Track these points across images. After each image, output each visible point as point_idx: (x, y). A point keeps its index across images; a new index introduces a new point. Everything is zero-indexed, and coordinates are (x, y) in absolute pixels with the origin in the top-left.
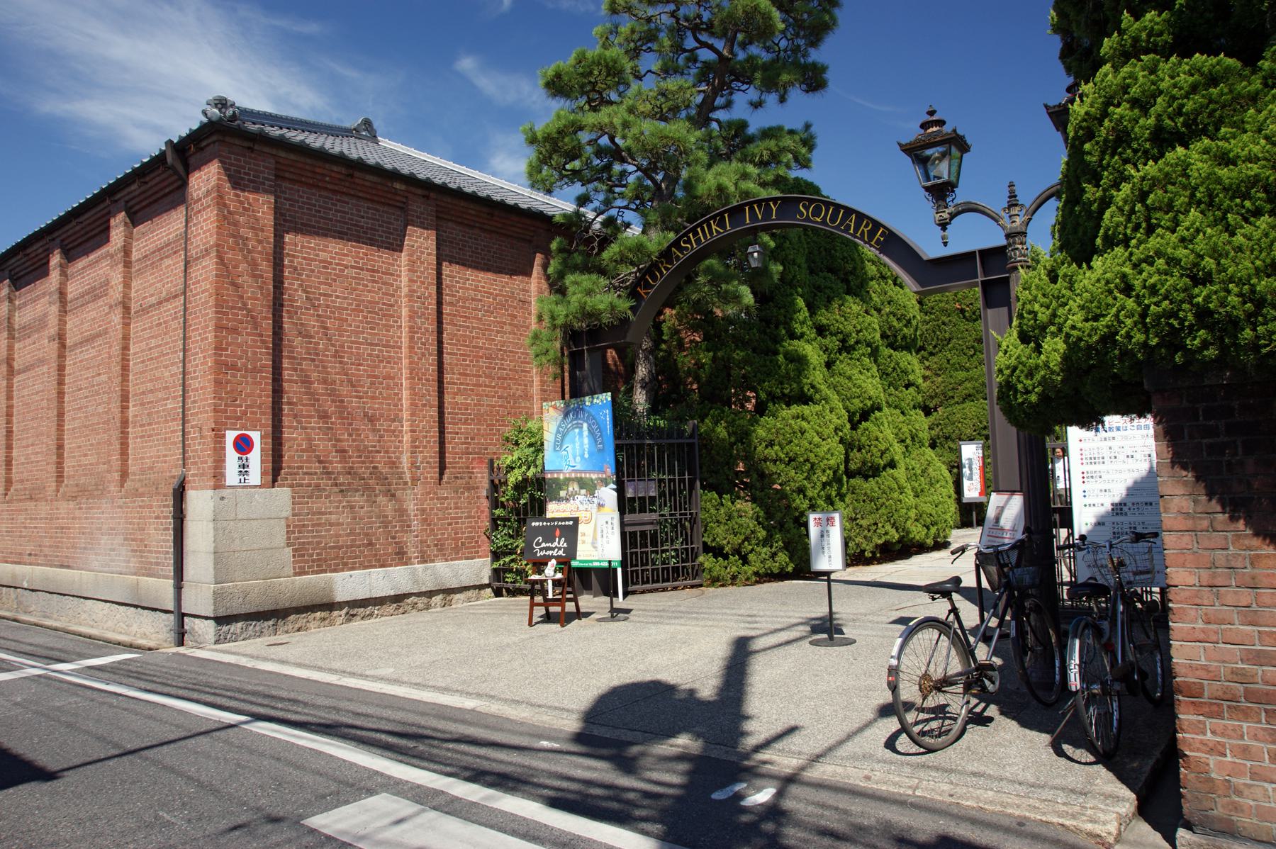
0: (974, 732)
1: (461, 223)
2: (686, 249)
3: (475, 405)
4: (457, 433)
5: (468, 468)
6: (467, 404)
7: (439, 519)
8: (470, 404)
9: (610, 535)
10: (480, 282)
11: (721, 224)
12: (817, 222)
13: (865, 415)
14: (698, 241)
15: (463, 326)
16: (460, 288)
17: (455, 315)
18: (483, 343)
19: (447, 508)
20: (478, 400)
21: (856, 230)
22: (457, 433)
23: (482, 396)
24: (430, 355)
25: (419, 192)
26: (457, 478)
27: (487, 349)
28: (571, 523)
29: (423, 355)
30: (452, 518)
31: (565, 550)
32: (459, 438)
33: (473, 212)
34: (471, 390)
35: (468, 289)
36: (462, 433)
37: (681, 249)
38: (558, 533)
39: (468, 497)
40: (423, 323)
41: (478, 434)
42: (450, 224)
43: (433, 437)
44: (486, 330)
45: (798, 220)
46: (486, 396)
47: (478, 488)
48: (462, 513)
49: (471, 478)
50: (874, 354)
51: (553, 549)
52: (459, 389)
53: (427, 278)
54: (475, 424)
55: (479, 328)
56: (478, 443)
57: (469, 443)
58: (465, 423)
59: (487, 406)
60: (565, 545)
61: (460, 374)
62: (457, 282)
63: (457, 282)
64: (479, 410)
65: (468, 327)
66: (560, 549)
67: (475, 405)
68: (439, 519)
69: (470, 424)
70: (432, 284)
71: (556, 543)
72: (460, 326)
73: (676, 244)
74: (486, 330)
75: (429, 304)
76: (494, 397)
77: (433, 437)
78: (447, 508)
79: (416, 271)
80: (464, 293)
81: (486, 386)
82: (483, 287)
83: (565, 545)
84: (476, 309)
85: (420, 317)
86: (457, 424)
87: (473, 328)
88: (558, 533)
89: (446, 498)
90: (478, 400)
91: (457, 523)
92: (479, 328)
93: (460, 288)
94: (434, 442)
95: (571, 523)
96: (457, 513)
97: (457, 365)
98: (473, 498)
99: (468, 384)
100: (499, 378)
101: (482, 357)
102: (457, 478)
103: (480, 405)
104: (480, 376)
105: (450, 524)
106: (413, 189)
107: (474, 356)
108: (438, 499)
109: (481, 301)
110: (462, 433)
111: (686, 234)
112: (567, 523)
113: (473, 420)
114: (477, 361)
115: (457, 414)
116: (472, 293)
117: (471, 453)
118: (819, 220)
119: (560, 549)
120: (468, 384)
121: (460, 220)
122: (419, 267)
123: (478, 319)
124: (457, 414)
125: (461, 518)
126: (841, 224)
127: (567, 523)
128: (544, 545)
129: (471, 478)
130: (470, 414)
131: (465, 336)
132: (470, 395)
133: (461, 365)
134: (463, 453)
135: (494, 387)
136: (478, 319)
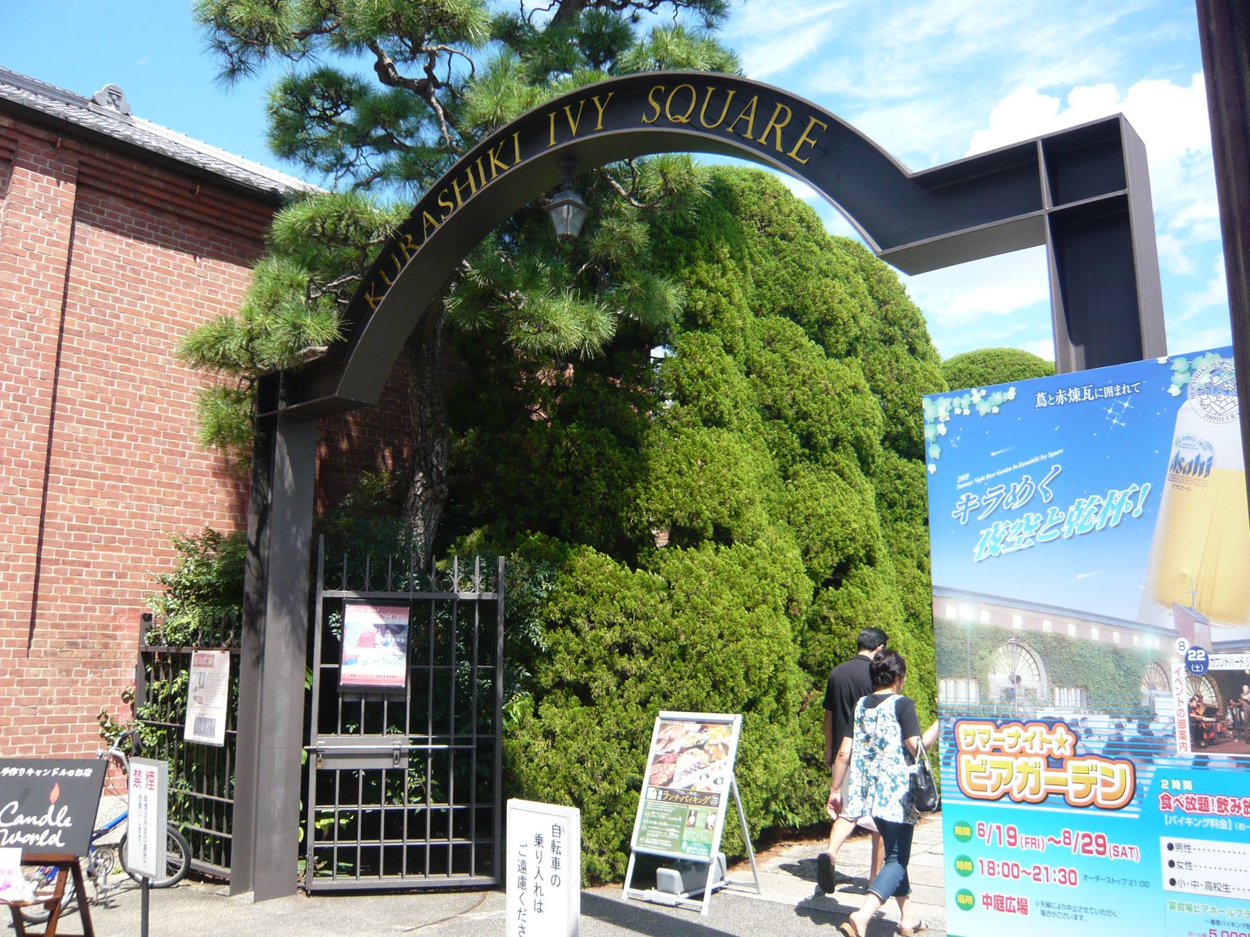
0: (1072, 920)
1: (136, 202)
2: (446, 210)
3: (133, 516)
4: (88, 565)
5: (105, 627)
6: (114, 513)
7: (20, 721)
8: (122, 514)
9: (546, 885)
10: (167, 304)
11: (506, 157)
12: (680, 125)
13: (841, 573)
14: (466, 193)
15: (122, 377)
16: (123, 311)
17: (105, 356)
18: (161, 409)
19: (41, 702)
20: (139, 508)
21: (758, 132)
22: (88, 565)
23: (149, 500)
24: (32, 419)
25: (43, 134)
26: (75, 645)
27: (168, 419)
28: (88, 772)
29: (18, 418)
30: (51, 720)
31: (66, 835)
32: (89, 574)
33: (161, 185)
34: (126, 489)
35: (139, 314)
36: (97, 565)
37: (437, 212)
38: (55, 794)
39: (93, 682)
40: (22, 362)
41: (135, 568)
42: (112, 201)
43: (23, 568)
44: (171, 387)
45: (645, 124)
46: (160, 501)
47: (116, 665)
48: (76, 710)
49: (106, 646)
50: (865, 462)
51: (38, 830)
52: (99, 486)
53: (44, 284)
54: (129, 550)
55: (158, 384)
56: (135, 585)
57: (114, 584)
58: (105, 548)
59: (160, 518)
60: (67, 823)
61: (105, 459)
62: (116, 300)
63: (116, 300)
64: (142, 525)
65: (132, 379)
66: (54, 830)
67: (133, 516)
68: (20, 721)
69: (119, 549)
70: (53, 296)
71: (48, 818)
72: (114, 376)
73: (428, 204)
74: (171, 387)
75: (45, 330)
76: (177, 503)
77: (23, 568)
78: (41, 702)
79: (21, 271)
80: (131, 320)
81: (160, 484)
82: (174, 314)
83: (67, 823)
84: (155, 350)
85: (19, 352)
86: (89, 547)
87: (143, 381)
88: (55, 794)
89: (43, 683)
90: (139, 508)
91: (60, 730)
92: (158, 384)
93: (123, 311)
94: (24, 578)
95: (88, 772)
96: (63, 710)
97: (99, 443)
98: (106, 683)
99: (121, 479)
100: (190, 472)
101: (157, 434)
102: (75, 645)
103: (144, 516)
104: (151, 466)
105: (43, 731)
106: (24, 127)
107: (139, 431)
108: (20, 683)
109: (166, 336)
110: (97, 565)
111: (446, 182)
112: (79, 773)
113: (125, 542)
114: (146, 440)
115: (91, 530)
116: (148, 323)
117: (115, 602)
118: (683, 120)
119: (54, 830)
120: (121, 479)
121: (132, 195)
122: (29, 264)
123: (156, 367)
124: (91, 530)
125: (73, 719)
126: (726, 123)
127: (79, 773)
128: (20, 820)
129: (106, 646)
130: (120, 532)
131: (123, 394)
132: (123, 498)
133: (109, 443)
134: (95, 601)
135: (179, 487)
136: (156, 367)
